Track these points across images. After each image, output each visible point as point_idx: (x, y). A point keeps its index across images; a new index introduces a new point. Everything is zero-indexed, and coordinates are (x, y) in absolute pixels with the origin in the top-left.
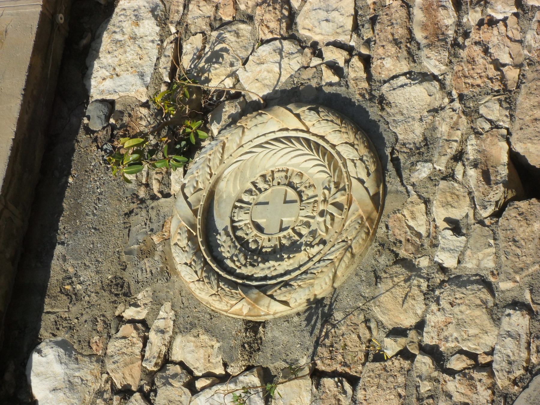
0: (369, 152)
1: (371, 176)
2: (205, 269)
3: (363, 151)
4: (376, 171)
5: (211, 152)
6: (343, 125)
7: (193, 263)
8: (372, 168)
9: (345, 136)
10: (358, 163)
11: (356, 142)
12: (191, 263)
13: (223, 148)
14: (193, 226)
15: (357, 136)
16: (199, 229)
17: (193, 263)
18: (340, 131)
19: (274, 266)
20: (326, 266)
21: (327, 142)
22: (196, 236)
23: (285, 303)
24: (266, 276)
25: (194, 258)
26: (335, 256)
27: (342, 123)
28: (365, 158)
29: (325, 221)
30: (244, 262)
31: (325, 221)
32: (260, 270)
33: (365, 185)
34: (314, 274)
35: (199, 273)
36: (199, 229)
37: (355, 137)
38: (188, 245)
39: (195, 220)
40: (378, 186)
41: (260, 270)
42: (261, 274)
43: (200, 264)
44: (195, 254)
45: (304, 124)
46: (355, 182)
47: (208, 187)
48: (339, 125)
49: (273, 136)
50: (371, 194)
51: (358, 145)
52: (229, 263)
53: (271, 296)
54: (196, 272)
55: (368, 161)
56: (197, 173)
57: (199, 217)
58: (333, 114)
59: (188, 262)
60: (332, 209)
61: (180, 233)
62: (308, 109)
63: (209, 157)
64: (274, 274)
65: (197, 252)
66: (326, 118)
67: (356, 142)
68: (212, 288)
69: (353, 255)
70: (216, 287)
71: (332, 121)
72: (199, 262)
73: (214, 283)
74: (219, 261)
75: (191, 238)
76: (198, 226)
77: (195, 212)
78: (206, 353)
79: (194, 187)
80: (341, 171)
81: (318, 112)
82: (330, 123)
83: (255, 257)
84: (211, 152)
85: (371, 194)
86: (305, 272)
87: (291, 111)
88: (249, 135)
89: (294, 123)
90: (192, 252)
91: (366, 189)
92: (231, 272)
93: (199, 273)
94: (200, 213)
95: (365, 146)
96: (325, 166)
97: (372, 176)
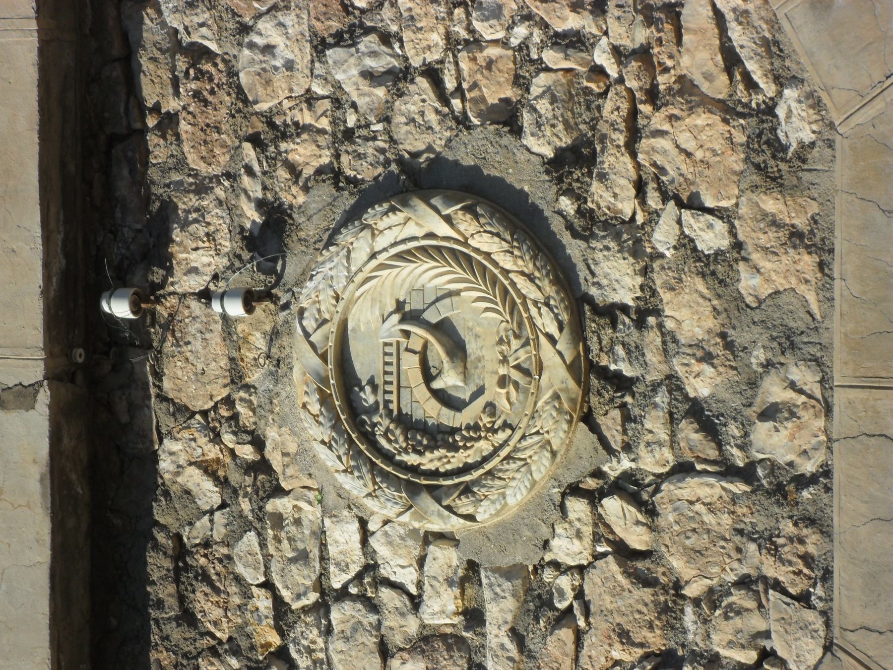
0: (557, 292)
1: (566, 330)
2: (351, 453)
3: (550, 290)
4: (571, 322)
5: (332, 265)
6: (515, 244)
7: (333, 443)
8: (565, 317)
9: (520, 262)
10: (544, 309)
11: (537, 274)
12: (330, 442)
13: (348, 257)
14: (324, 380)
15: (538, 264)
16: (339, 406)
17: (333, 443)
18: (512, 253)
19: (446, 457)
20: (518, 470)
21: (495, 264)
22: (331, 395)
23: (471, 518)
24: (437, 469)
25: (333, 434)
26: (528, 455)
27: (513, 239)
28: (552, 302)
29: (508, 393)
30: (404, 445)
31: (508, 393)
32: (429, 461)
33: (557, 347)
34: (504, 479)
35: (344, 459)
36: (339, 406)
37: (535, 264)
38: (322, 413)
39: (326, 371)
40: (576, 347)
41: (429, 461)
42: (432, 466)
43: (343, 444)
44: (333, 428)
45: (459, 232)
46: (543, 340)
47: (337, 318)
48: (509, 243)
49: (415, 244)
50: (568, 362)
51: (539, 279)
52: (383, 442)
53: (449, 508)
54: (339, 458)
55: (557, 307)
56: (317, 296)
57: (330, 366)
58: (500, 221)
59: (327, 440)
60: (516, 375)
61: (306, 393)
62: (461, 209)
63: (330, 273)
64: (449, 467)
65: (336, 426)
66: (489, 228)
67: (537, 274)
68: (365, 485)
69: (554, 454)
70: (370, 484)
71: (498, 235)
72: (342, 442)
73: (368, 477)
74: (370, 439)
75: (325, 400)
76: (332, 382)
77: (324, 357)
78: (475, 94)
79: (316, 320)
80: (521, 316)
81: (476, 216)
82: (496, 239)
83: (419, 437)
84: (332, 265)
85: (568, 362)
86: (490, 473)
87: (438, 211)
88: (382, 242)
89: (443, 229)
90: (329, 424)
91: (560, 353)
92: (388, 458)
93: (344, 459)
94: (331, 356)
95: (550, 281)
96: (496, 304)
97: (566, 330)
